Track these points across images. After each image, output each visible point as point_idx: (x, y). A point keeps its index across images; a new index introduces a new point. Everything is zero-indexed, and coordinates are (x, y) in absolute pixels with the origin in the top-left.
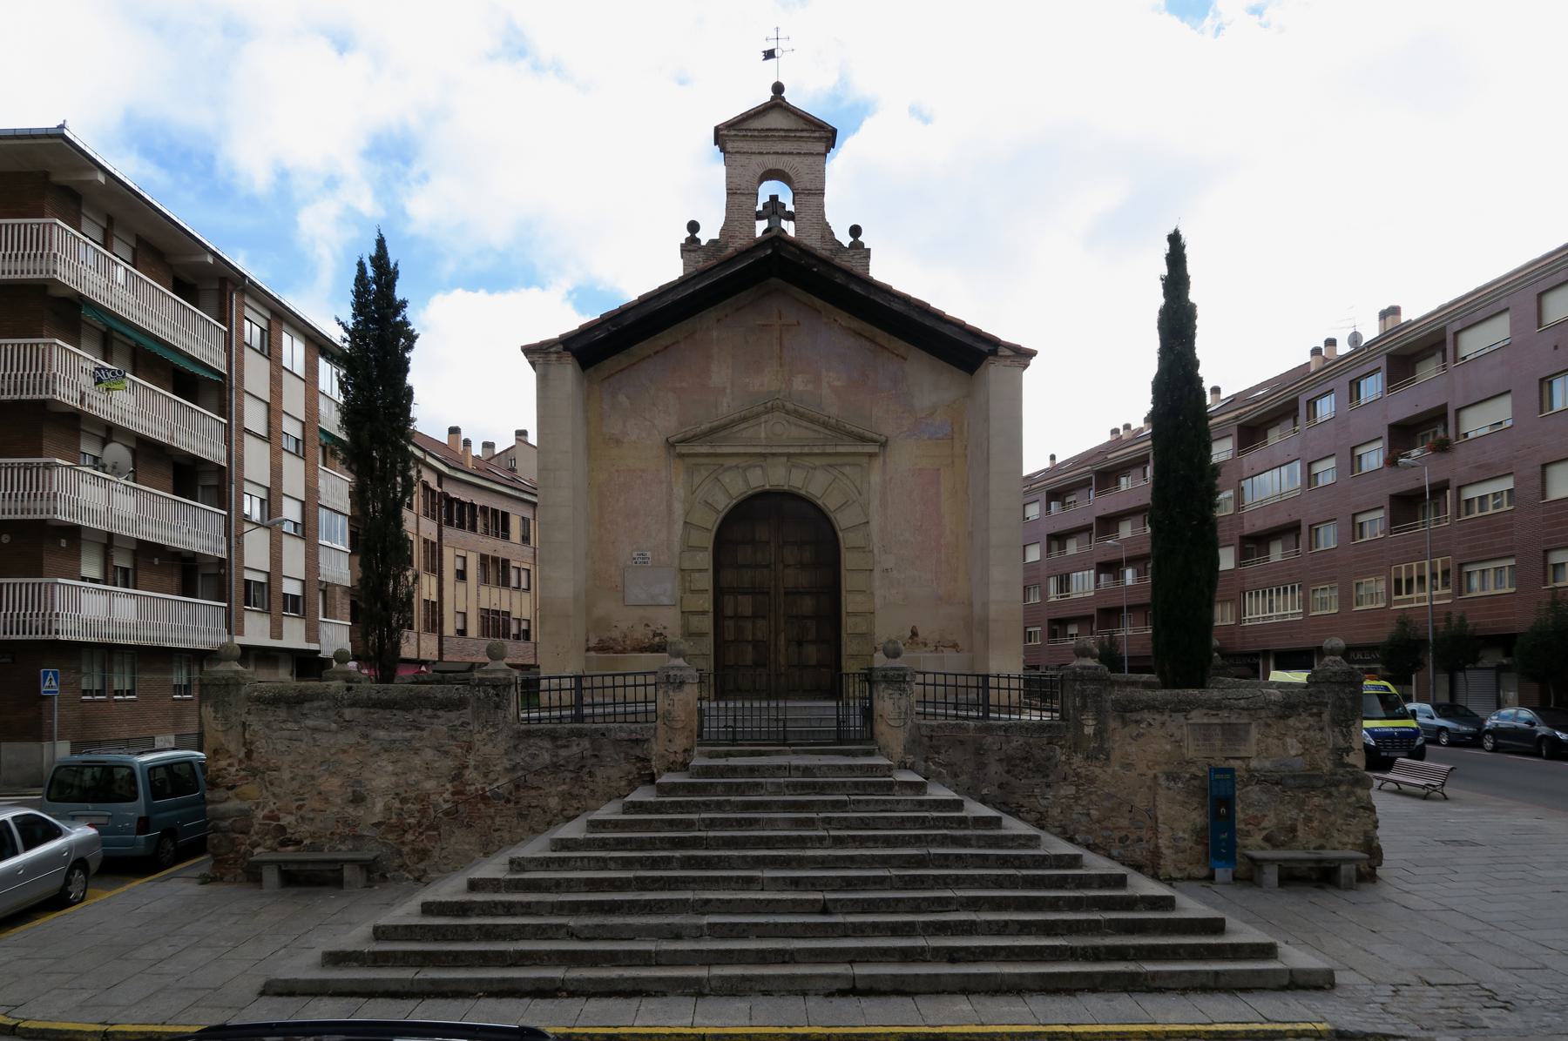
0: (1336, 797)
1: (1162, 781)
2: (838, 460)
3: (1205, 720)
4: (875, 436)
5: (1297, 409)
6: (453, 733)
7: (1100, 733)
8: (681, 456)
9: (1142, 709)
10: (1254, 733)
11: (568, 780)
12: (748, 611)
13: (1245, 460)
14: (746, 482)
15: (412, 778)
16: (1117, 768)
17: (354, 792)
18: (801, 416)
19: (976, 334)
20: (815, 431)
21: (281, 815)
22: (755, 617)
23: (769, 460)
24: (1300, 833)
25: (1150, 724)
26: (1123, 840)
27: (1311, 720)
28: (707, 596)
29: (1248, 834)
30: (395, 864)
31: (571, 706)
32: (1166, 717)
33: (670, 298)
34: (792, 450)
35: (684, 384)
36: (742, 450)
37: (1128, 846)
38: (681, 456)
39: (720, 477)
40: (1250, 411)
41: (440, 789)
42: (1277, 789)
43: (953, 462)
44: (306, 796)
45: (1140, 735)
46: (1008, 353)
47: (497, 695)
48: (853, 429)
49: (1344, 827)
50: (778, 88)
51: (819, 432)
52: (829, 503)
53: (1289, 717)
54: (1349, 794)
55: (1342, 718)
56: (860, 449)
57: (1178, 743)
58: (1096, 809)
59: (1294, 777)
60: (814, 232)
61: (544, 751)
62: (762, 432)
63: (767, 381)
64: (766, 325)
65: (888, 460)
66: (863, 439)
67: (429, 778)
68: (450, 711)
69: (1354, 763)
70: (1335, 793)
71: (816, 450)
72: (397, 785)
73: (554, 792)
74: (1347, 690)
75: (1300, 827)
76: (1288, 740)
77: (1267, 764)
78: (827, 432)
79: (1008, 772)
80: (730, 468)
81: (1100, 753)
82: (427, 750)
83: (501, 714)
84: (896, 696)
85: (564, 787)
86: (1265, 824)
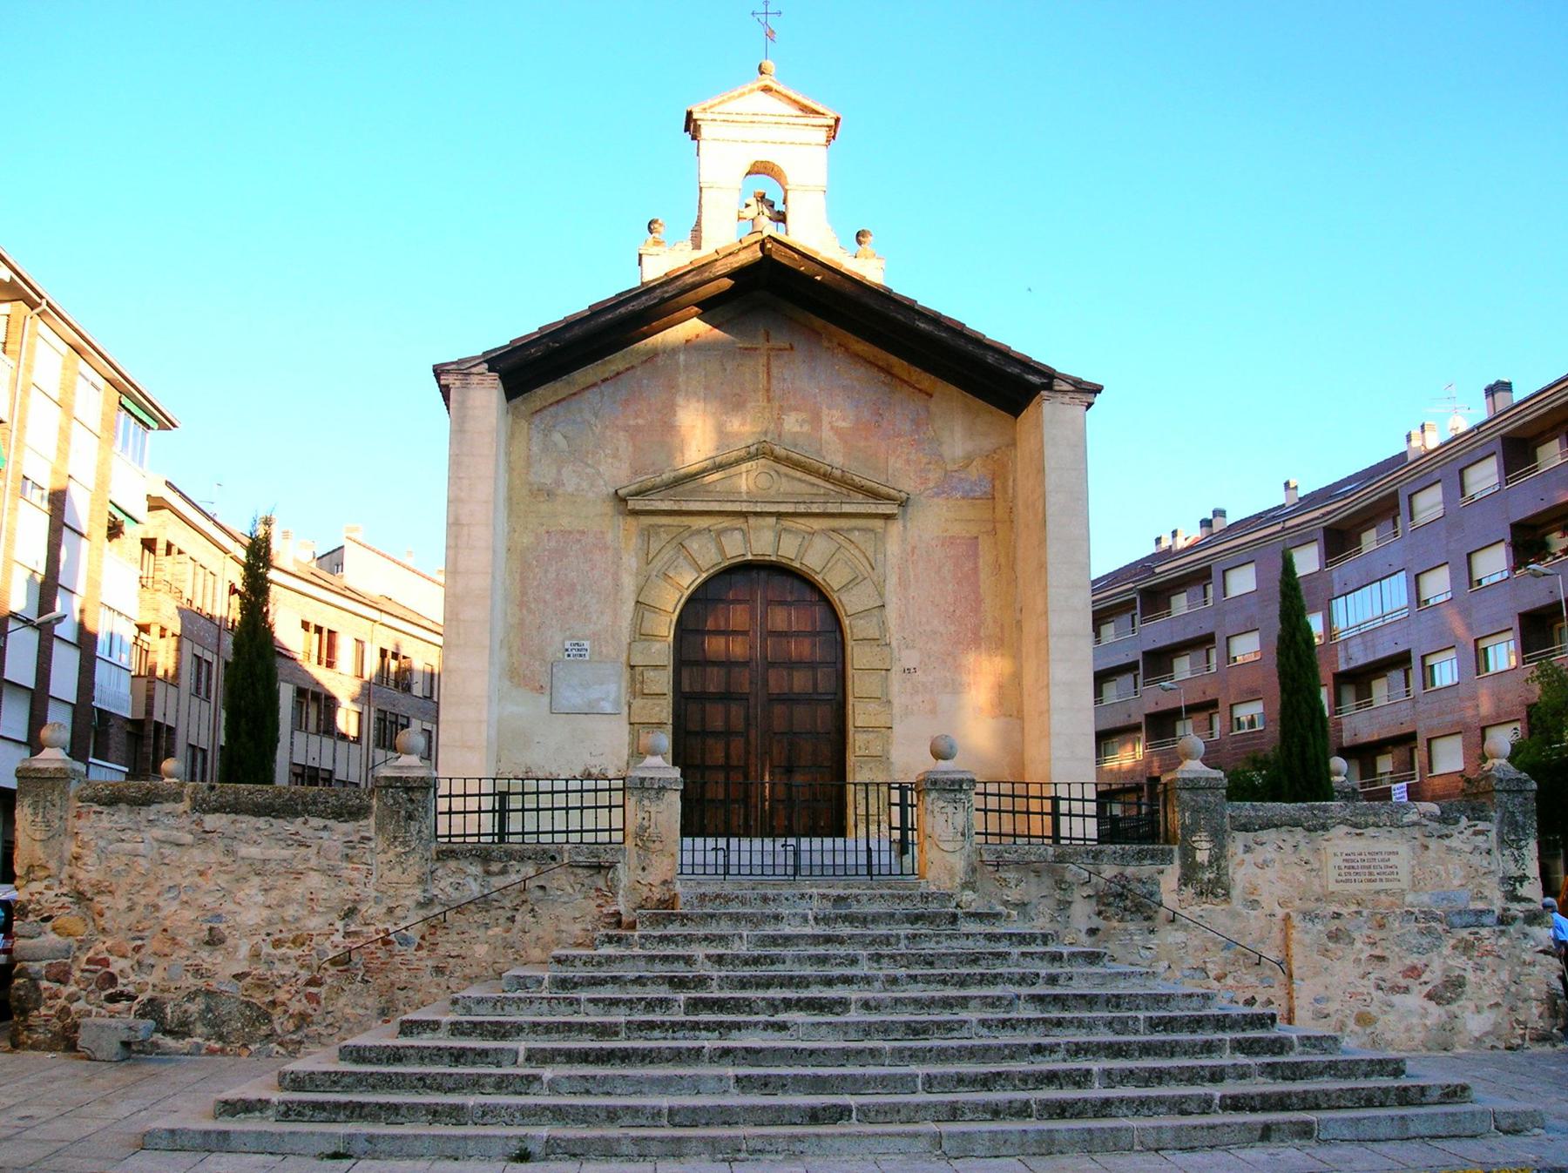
1: (1296, 919)
4: (892, 492)
5: (1398, 506)
6: (349, 851)
7: (1217, 859)
8: (635, 513)
11: (502, 921)
13: (1335, 575)
14: (721, 550)
15: (290, 911)
17: (211, 929)
18: (797, 465)
19: (1026, 364)
20: (813, 485)
21: (112, 959)
30: (262, 1032)
31: (493, 834)
33: (577, 331)
34: (783, 508)
35: (640, 421)
36: (716, 507)
38: (635, 513)
39: (686, 543)
40: (1339, 508)
41: (327, 929)
43: (994, 529)
44: (146, 933)
46: (1066, 387)
47: (411, 801)
48: (864, 482)
52: (833, 579)
55: (1513, 837)
56: (872, 509)
61: (470, 879)
64: (751, 349)
65: (909, 525)
66: (875, 495)
67: (313, 911)
68: (346, 821)
71: (815, 509)
72: (270, 922)
73: (482, 938)
79: (1099, 913)
80: (699, 532)
82: (312, 873)
83: (414, 827)
84: (950, 809)
85: (497, 930)
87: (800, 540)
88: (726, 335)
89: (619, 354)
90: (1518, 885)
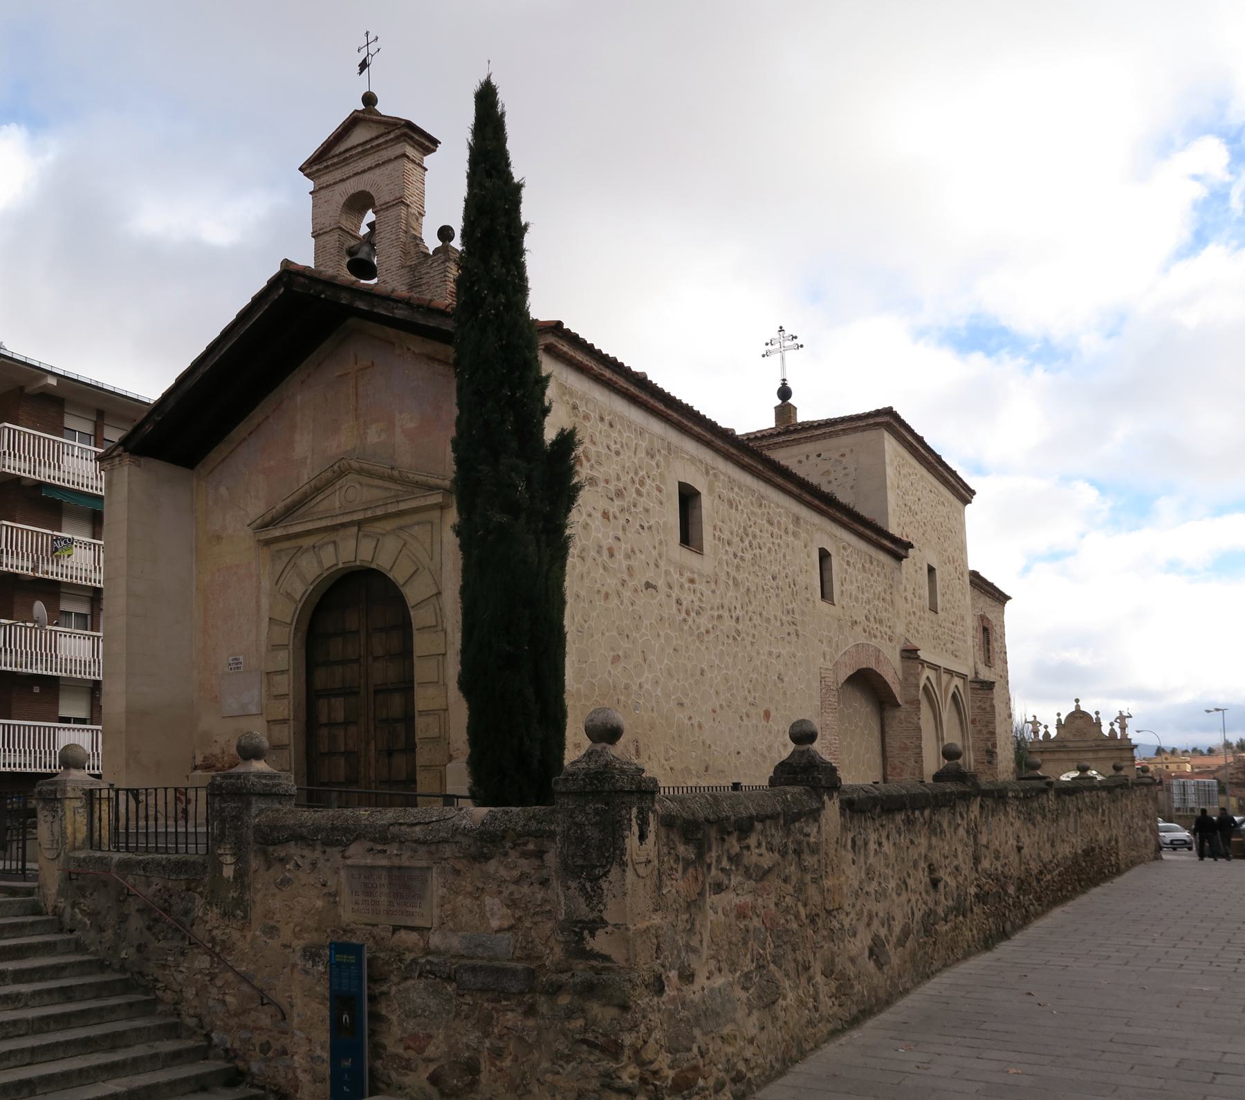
0: (543, 1017)
2: (407, 520)
3: (369, 861)
9: (288, 840)
10: (436, 887)
12: (340, 716)
16: (258, 933)
18: (370, 474)
20: (386, 489)
22: (347, 723)
23: (341, 533)
24: (483, 1077)
25: (298, 866)
26: (265, 1048)
27: (525, 865)
28: (286, 701)
29: (407, 1066)
32: (318, 854)
33: (203, 370)
36: (310, 526)
37: (270, 1060)
42: (450, 988)
45: (286, 882)
49: (549, 1077)
50: (369, 99)
51: (390, 489)
53: (487, 858)
54: (570, 1014)
55: (580, 862)
57: (332, 897)
58: (234, 996)
59: (474, 969)
60: (394, 250)
62: (333, 503)
63: (342, 442)
69: (606, 950)
70: (544, 1008)
74: (590, 808)
75: (484, 1066)
76: (488, 900)
77: (455, 942)
78: (399, 487)
79: (149, 928)
81: (237, 910)
86: (430, 1051)
87: (375, 543)
88: (36, 386)
89: (258, 409)
90: (586, 933)
